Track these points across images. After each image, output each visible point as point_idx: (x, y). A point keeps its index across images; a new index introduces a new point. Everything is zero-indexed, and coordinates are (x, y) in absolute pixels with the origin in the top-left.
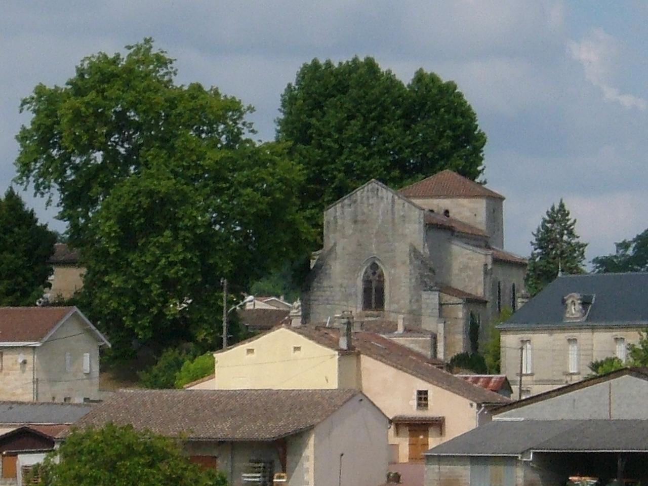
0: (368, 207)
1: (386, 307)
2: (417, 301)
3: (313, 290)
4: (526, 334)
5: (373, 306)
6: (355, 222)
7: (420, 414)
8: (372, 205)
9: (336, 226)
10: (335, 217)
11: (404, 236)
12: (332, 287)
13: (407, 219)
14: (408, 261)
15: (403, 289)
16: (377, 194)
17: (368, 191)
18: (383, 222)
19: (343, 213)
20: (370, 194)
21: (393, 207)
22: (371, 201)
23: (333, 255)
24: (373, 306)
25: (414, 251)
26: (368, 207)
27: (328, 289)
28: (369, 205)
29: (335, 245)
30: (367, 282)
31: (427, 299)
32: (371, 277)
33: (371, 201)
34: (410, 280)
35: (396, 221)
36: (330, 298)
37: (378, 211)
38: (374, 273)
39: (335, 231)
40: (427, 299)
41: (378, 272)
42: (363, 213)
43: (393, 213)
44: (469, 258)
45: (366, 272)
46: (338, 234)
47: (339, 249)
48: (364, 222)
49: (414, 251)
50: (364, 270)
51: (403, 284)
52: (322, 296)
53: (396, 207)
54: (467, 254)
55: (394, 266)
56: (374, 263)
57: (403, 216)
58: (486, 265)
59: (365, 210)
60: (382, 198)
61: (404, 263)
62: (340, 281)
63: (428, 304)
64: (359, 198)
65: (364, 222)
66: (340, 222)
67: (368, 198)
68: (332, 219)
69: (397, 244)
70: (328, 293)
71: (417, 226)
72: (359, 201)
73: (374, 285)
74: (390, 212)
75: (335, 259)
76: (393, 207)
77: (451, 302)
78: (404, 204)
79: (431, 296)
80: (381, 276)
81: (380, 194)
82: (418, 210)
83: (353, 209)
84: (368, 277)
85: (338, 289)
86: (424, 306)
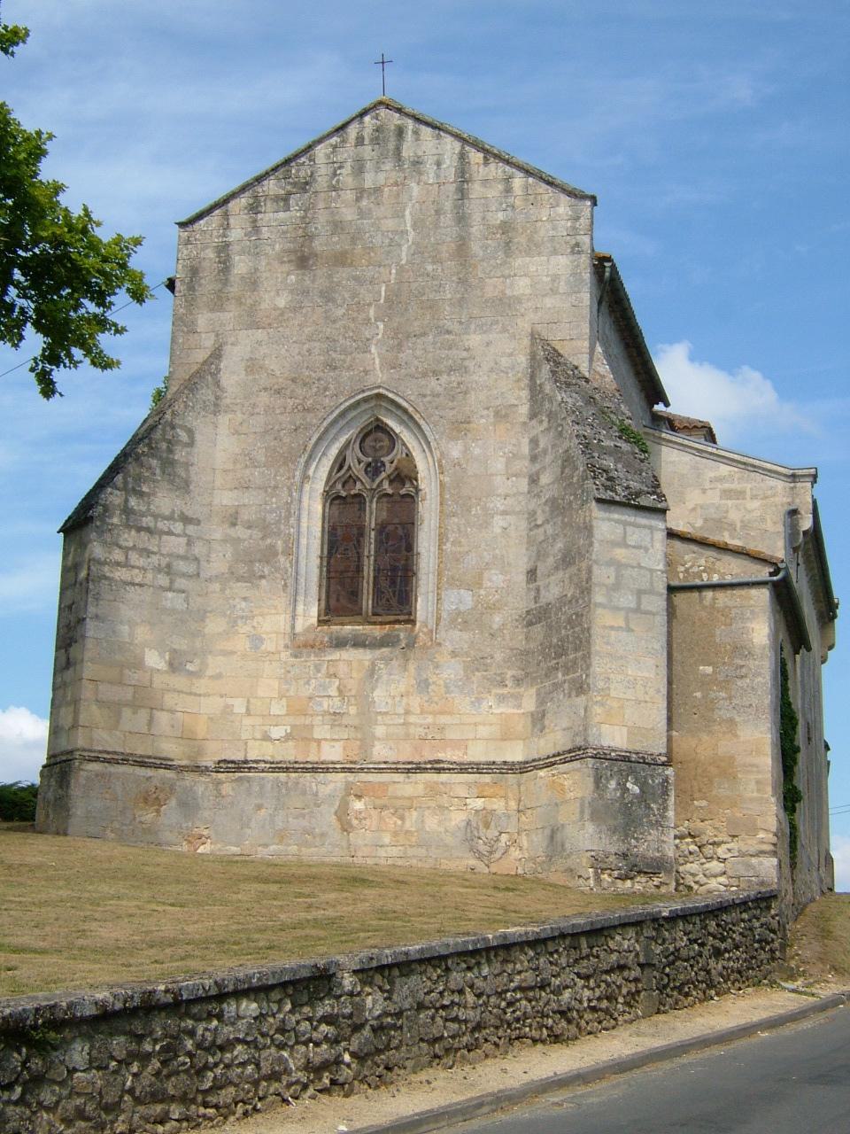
0: (358, 199)
1: (423, 606)
2: (567, 560)
3: (102, 517)
4: (467, 1100)
5: (367, 602)
6: (303, 260)
7: (700, 1020)
8: (377, 190)
9: (226, 282)
10: (224, 249)
11: (505, 305)
12: (198, 522)
13: (522, 239)
14: (524, 410)
15: (499, 522)
16: (398, 150)
17: (360, 141)
18: (418, 250)
19: (256, 228)
20: (367, 151)
21: (462, 194)
22: (369, 180)
23: (206, 394)
24: (367, 602)
25: (548, 358)
26: (358, 199)
27: (178, 527)
28: (361, 193)
29: (217, 354)
30: (342, 500)
31: (615, 544)
32: (364, 484)
33: (369, 180)
34: (534, 480)
35: (475, 247)
36: (181, 566)
37: (399, 215)
38: (374, 469)
39: (218, 303)
40: (615, 544)
41: (390, 462)
42: (337, 226)
43: (462, 219)
44: (727, 494)
45: (340, 462)
46: (229, 316)
47: (232, 375)
48: (341, 259)
49: (548, 358)
50: (334, 451)
51: (499, 504)
52: (147, 553)
53: (476, 190)
54: (720, 479)
55: (461, 427)
56: (380, 427)
57: (506, 227)
58: (793, 513)
59: (348, 214)
60: (417, 163)
61: (502, 415)
62: (226, 499)
63: (619, 566)
64: (323, 171)
65: (341, 259)
66: (241, 265)
67: (359, 169)
68: (210, 254)
69: (474, 340)
70: (175, 544)
71: (562, 263)
72: (322, 182)
73: (373, 515)
74: (447, 219)
75: (216, 408)
76: (462, 194)
77: (715, 579)
78: (508, 180)
79: (634, 537)
80: (405, 476)
81: (408, 151)
82: (564, 198)
83: (295, 213)
84: (350, 480)
85: (217, 532)
86: (603, 575)
